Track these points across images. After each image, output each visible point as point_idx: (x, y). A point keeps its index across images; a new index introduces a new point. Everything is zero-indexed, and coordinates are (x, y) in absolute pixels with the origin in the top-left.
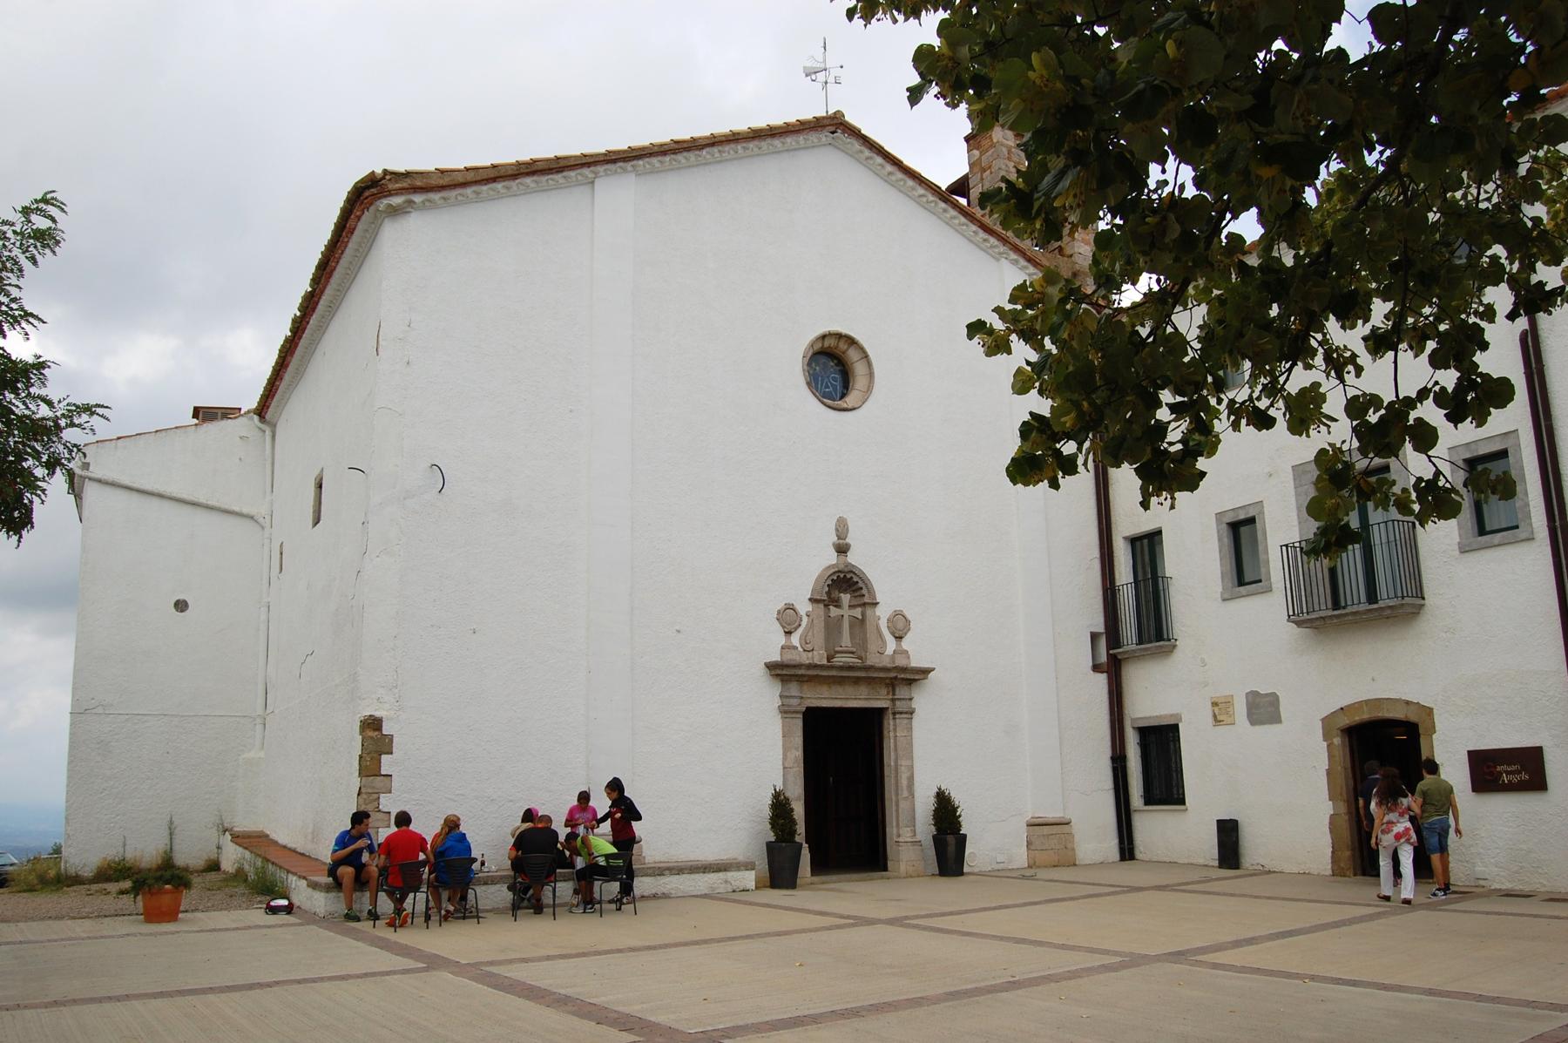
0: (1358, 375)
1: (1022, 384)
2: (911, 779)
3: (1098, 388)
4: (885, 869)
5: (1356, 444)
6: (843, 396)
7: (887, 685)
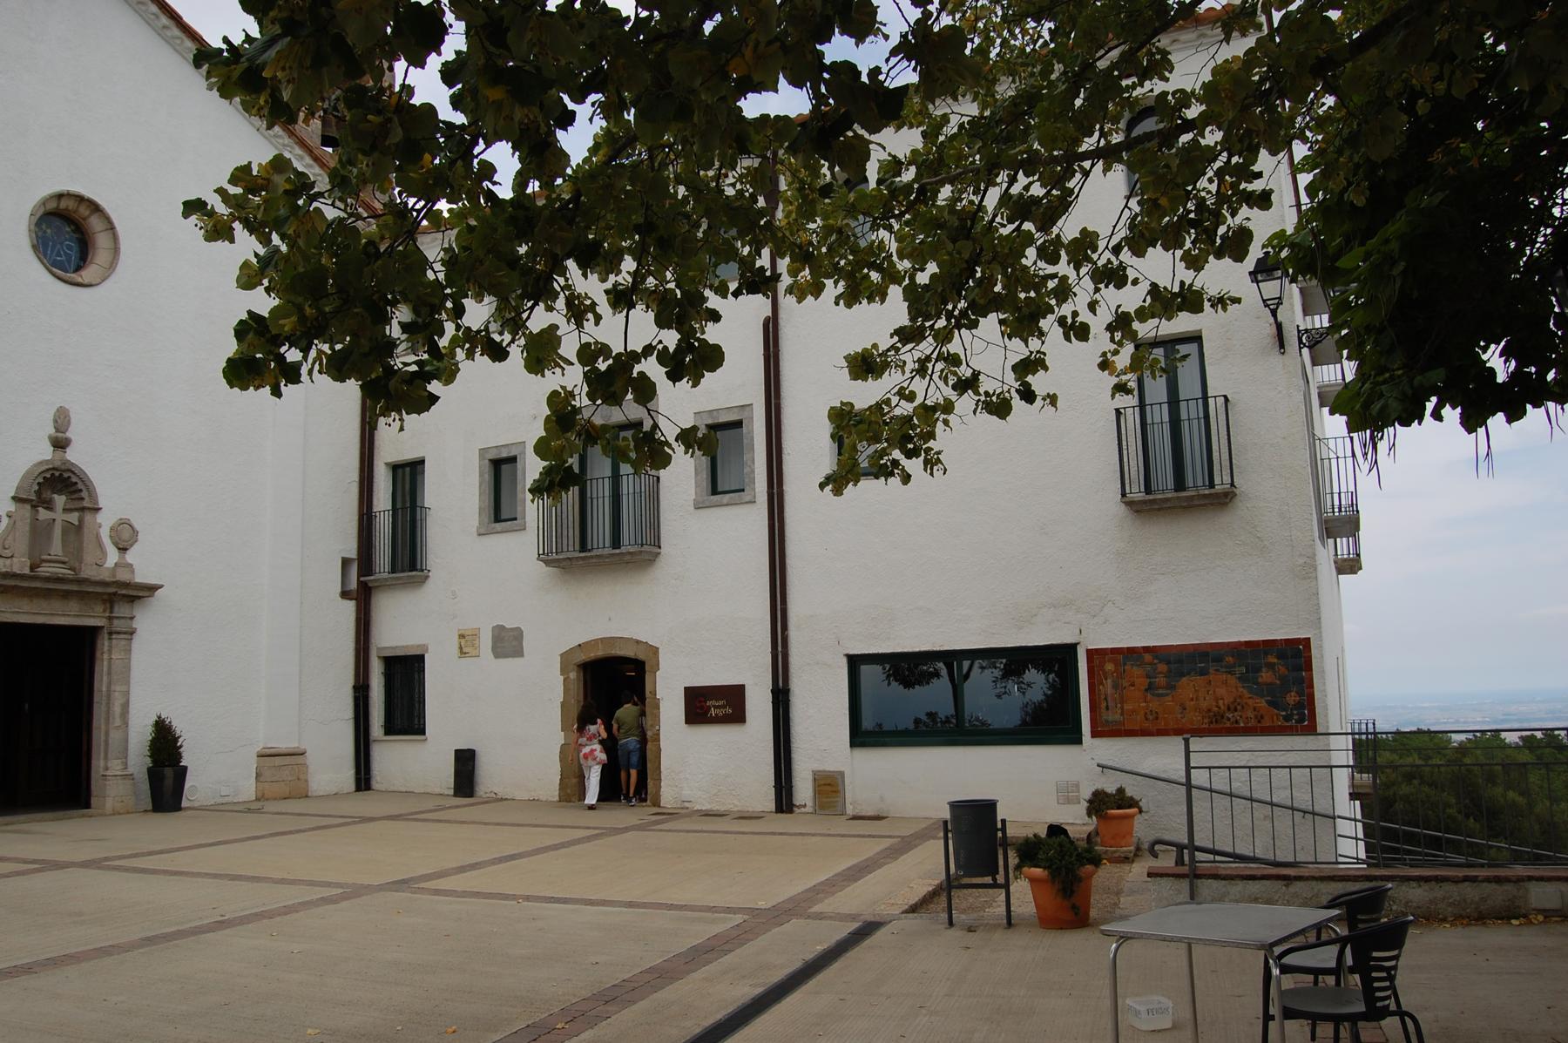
0: (597, 324)
1: (248, 278)
2: (126, 706)
3: (327, 295)
4: (88, 806)
5: (586, 388)
6: (78, 269)
7: (104, 601)
